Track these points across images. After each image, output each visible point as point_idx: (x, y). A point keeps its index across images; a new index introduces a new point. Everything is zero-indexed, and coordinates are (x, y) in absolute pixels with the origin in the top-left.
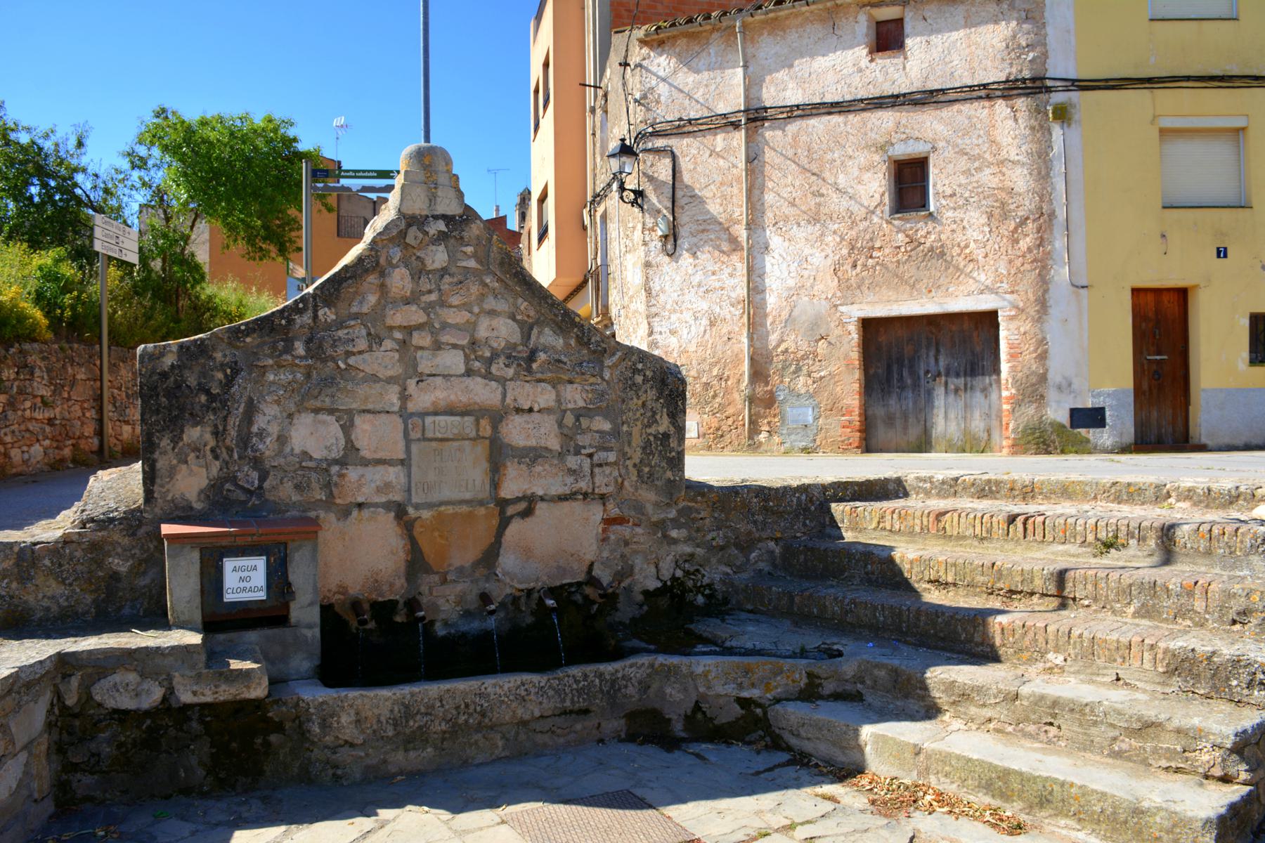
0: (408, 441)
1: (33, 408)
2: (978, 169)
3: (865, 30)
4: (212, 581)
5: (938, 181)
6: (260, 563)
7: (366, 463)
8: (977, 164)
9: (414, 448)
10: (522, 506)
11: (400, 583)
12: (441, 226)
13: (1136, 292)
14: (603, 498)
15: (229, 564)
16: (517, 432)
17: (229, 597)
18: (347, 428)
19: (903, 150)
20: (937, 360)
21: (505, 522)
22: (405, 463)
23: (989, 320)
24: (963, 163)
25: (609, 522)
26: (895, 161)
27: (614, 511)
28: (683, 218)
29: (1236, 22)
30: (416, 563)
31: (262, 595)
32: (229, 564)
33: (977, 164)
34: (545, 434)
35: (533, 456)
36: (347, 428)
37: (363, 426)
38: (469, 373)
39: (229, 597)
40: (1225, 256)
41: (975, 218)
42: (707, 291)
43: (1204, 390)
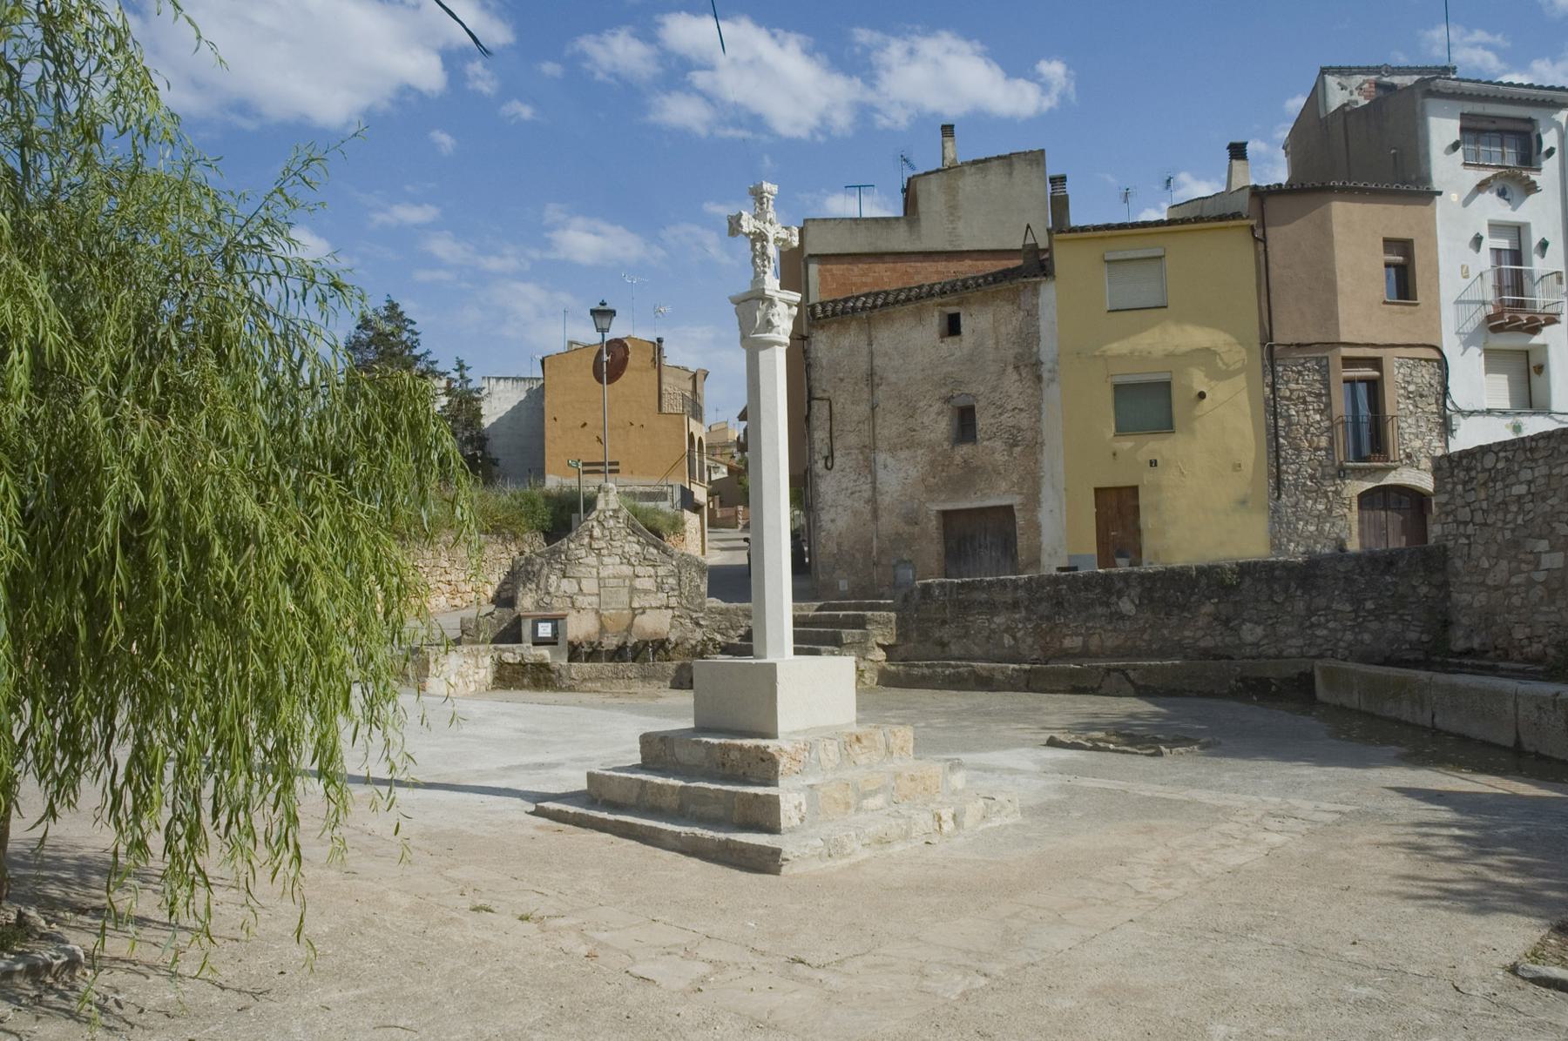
0: (600, 587)
1: (441, 575)
2: (1001, 414)
3: (937, 321)
4: (535, 630)
5: (983, 422)
6: (550, 625)
7: (585, 595)
8: (1000, 411)
9: (602, 590)
10: (640, 611)
11: (597, 636)
12: (611, 513)
13: (1098, 491)
14: (673, 608)
15: (540, 625)
16: (638, 583)
17: (540, 635)
18: (579, 584)
19: (961, 402)
20: (985, 538)
21: (634, 616)
22: (599, 595)
23: (1009, 509)
24: (992, 409)
25: (674, 617)
26: (959, 408)
27: (677, 613)
28: (837, 445)
29: (1164, 310)
30: (603, 629)
31: (550, 635)
32: (540, 625)
33: (1000, 411)
34: (648, 584)
35: (646, 592)
36: (579, 584)
37: (584, 583)
38: (622, 563)
39: (540, 635)
40: (1156, 465)
41: (998, 444)
42: (852, 493)
43: (1275, 545)
